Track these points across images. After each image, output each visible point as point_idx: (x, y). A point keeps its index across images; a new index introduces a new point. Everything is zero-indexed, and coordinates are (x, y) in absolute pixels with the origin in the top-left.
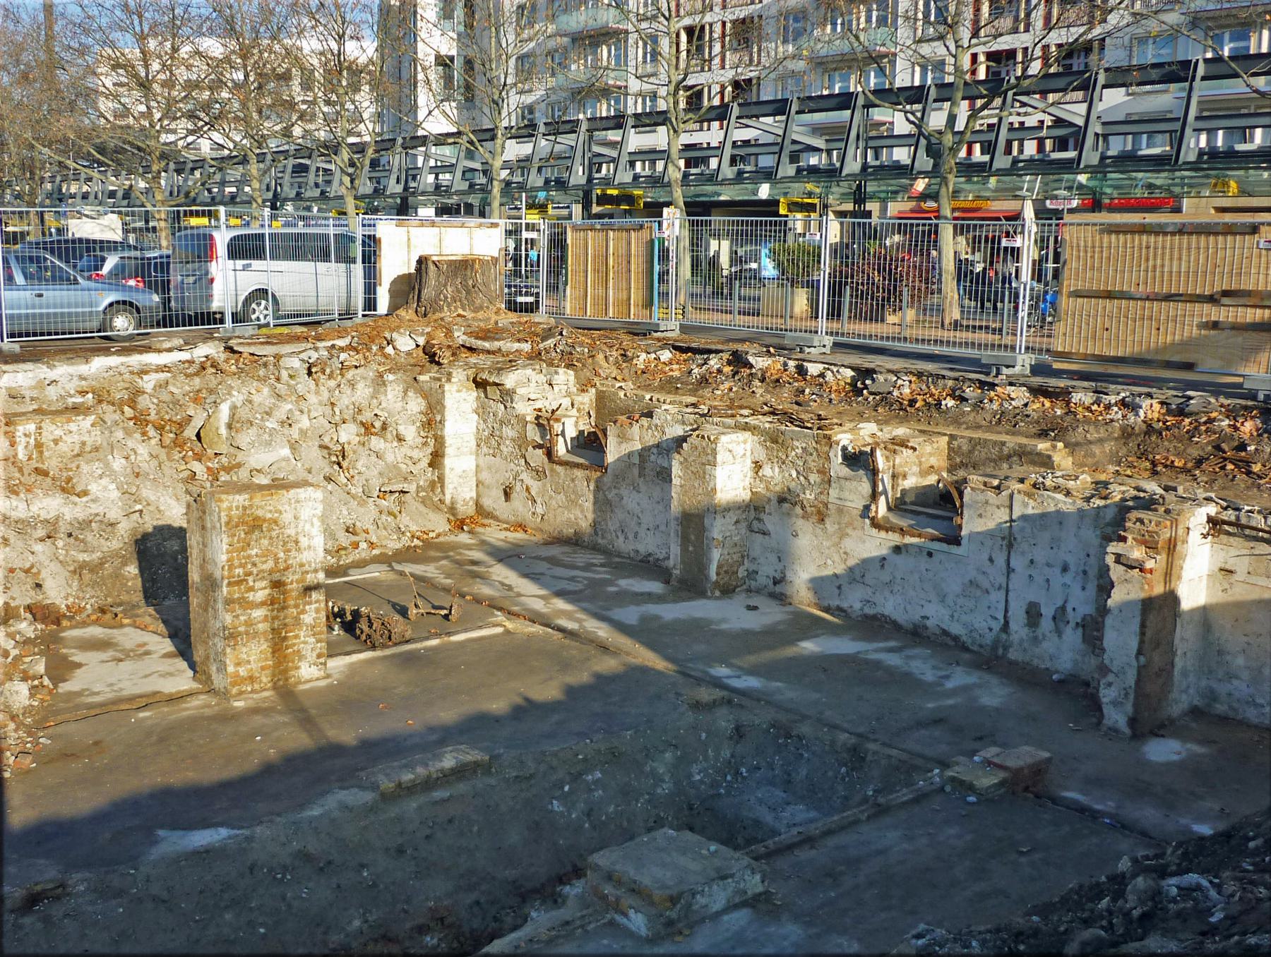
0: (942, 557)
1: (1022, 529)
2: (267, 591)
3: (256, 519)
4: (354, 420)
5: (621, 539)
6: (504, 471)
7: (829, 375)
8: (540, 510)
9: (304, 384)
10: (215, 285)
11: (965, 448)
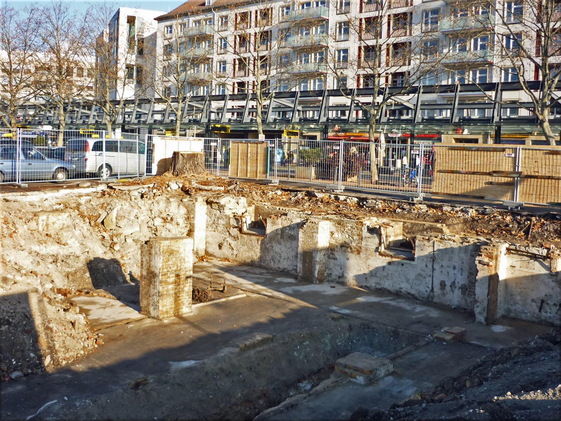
0: (408, 266)
1: (438, 254)
2: (174, 278)
3: (172, 250)
4: (159, 216)
5: (272, 263)
6: (218, 237)
7: (348, 200)
8: (235, 252)
9: (140, 202)
10: (87, 161)
11: (409, 226)
